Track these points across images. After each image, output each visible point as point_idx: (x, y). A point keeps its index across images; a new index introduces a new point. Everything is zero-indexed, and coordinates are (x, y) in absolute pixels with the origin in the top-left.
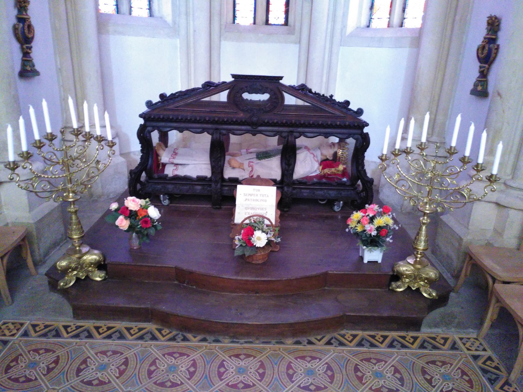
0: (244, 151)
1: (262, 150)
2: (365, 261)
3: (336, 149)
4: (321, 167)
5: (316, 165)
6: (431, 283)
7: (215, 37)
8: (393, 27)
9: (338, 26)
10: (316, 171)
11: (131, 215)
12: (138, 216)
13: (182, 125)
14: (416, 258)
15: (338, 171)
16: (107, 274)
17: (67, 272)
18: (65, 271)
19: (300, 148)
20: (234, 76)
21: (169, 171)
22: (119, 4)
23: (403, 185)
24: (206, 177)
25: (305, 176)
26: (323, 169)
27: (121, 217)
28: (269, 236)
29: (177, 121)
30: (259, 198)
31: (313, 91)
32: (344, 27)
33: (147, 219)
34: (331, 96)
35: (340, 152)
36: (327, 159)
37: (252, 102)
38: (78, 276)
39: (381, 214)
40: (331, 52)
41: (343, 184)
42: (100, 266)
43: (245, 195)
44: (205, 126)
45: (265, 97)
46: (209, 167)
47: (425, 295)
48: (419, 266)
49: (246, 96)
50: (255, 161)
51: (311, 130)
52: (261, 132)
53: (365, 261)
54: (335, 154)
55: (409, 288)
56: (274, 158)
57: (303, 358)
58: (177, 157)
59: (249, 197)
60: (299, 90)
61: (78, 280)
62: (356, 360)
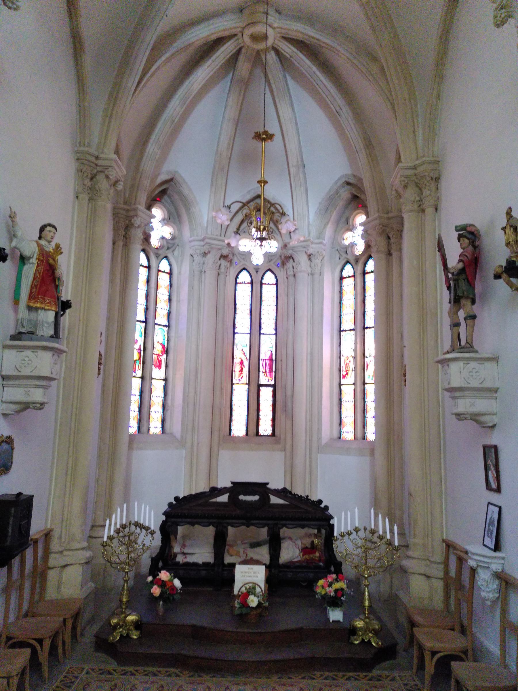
0: (239, 542)
1: (255, 541)
2: (331, 621)
3: (313, 539)
4: (301, 554)
5: (297, 552)
6: (376, 633)
7: (215, 447)
8: (357, 439)
9: (315, 438)
10: (298, 557)
11: (162, 584)
12: (166, 586)
13: (195, 520)
14: (365, 614)
15: (315, 557)
16: (141, 633)
17: (116, 628)
18: (115, 628)
19: (284, 539)
20: (232, 483)
21: (180, 559)
22: (140, 426)
23: (350, 558)
24: (210, 563)
25: (289, 561)
26: (303, 555)
27: (155, 586)
28: (259, 599)
29: (186, 517)
30: (252, 574)
31: (293, 493)
32: (319, 439)
33: (173, 588)
34: (307, 496)
35: (316, 541)
36: (307, 548)
37: (246, 502)
38: (122, 633)
39: (337, 580)
40: (311, 458)
41: (319, 567)
42: (137, 625)
43: (242, 572)
44: (211, 520)
45: (256, 498)
46: (213, 555)
47: (374, 644)
48: (367, 620)
49: (242, 497)
50: (248, 549)
51: (291, 522)
52: (253, 525)
53: (331, 621)
54: (313, 542)
55: (363, 640)
56: (264, 546)
57: (284, 685)
58: (186, 548)
59: (245, 574)
60: (281, 492)
61: (122, 636)
62: (320, 686)
